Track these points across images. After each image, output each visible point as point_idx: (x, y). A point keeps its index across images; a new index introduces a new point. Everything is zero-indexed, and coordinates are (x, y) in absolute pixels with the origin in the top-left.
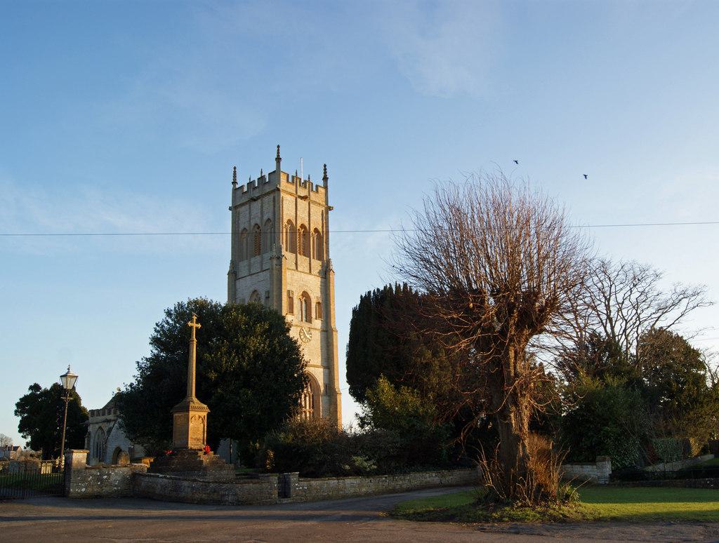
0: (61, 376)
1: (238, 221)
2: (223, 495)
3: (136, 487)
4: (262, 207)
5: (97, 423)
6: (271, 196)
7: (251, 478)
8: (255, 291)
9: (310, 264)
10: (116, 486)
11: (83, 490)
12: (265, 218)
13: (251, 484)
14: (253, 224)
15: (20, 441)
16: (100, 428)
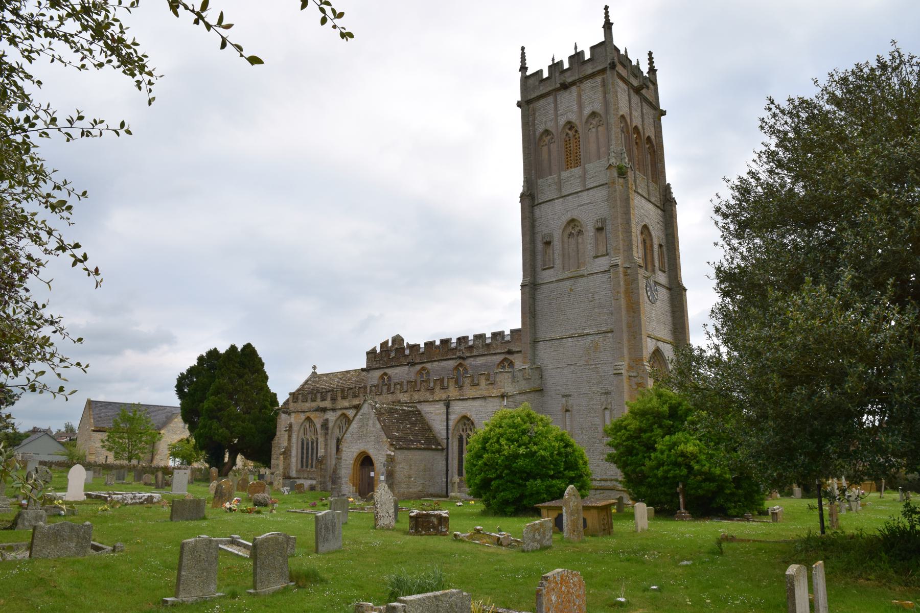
1: (534, 120)
5: (304, 412)
6: (599, 79)
8: (573, 220)
12: (587, 111)
14: (562, 121)
16: (308, 419)
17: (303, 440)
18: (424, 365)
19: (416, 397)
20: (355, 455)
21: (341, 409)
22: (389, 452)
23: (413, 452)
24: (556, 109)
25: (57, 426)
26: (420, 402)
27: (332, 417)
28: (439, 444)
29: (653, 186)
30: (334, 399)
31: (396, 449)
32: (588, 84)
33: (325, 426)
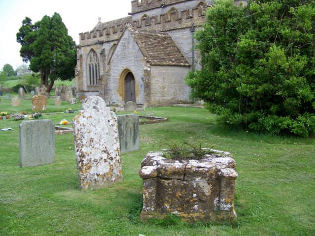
5: (89, 46)
15: (18, 63)
16: (92, 50)
17: (90, 65)
18: (173, 6)
19: (167, 27)
20: (120, 72)
21: (113, 41)
22: (145, 69)
23: (165, 68)
25: (191, 89)
26: (170, 30)
27: (107, 47)
28: (186, 62)
30: (108, 34)
31: (151, 65)
33: (102, 53)
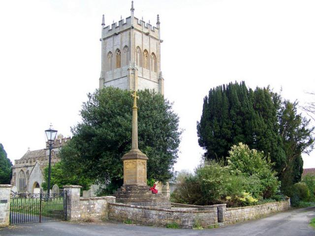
0: (46, 131)
2: (184, 222)
3: (111, 213)
4: (121, 39)
6: (128, 32)
7: (202, 210)
9: (150, 74)
10: (98, 213)
11: (79, 216)
12: (124, 45)
13: (203, 213)
14: (115, 49)
16: (22, 170)
24: (113, 43)
29: (153, 73)
32: (124, 34)
